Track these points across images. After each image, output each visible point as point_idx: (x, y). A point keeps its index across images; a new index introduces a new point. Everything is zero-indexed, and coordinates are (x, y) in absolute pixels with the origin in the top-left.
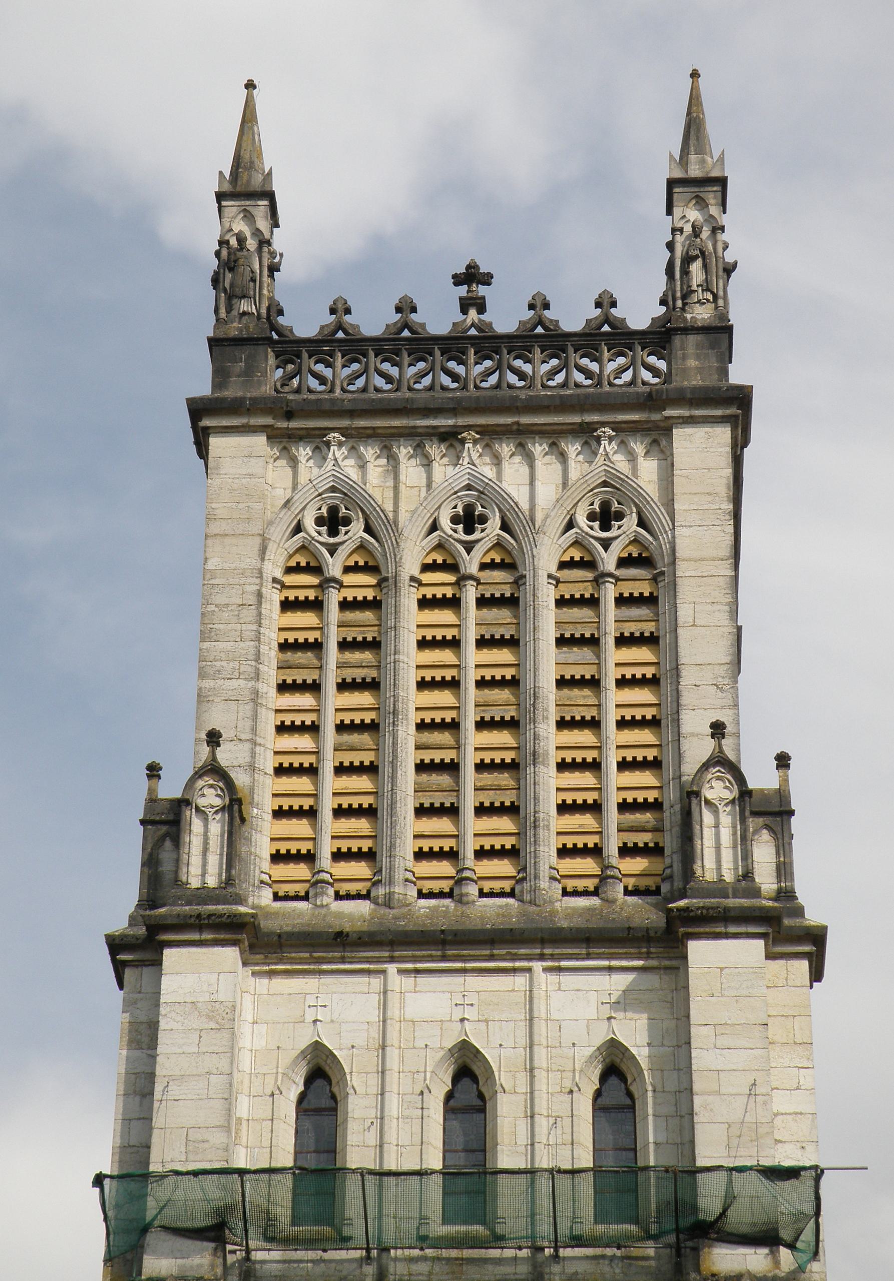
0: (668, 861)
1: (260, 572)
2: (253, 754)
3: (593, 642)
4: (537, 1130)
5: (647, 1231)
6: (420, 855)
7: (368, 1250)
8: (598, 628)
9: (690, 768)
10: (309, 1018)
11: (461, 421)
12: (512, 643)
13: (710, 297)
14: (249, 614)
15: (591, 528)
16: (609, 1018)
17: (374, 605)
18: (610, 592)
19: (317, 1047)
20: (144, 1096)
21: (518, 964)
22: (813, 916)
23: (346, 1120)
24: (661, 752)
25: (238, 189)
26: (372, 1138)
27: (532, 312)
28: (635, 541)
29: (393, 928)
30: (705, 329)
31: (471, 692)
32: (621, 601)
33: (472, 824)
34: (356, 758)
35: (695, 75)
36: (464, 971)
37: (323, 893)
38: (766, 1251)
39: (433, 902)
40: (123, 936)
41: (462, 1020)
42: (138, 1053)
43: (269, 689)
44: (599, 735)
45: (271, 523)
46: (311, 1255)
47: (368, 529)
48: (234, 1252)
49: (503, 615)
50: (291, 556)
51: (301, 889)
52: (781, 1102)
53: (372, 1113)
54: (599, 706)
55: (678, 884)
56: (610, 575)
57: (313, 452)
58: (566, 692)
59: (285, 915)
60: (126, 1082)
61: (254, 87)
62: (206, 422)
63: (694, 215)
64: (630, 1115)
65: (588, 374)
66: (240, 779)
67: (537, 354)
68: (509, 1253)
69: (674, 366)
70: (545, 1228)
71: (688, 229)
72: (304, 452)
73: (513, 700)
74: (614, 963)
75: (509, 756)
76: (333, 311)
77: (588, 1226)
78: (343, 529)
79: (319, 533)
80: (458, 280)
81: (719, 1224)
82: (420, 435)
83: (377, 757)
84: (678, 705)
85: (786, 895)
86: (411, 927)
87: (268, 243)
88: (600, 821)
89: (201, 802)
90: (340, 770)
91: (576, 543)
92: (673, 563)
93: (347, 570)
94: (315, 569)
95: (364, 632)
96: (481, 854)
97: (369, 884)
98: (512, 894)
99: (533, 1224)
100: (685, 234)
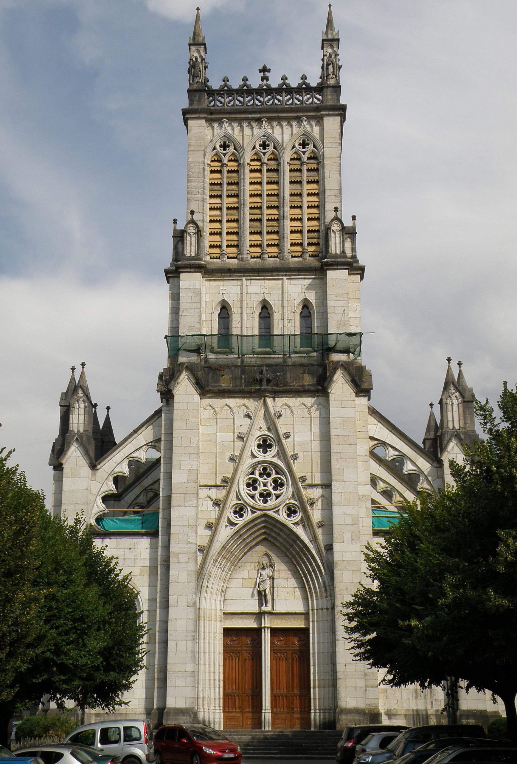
0: (321, 247)
1: (204, 162)
2: (203, 217)
3: (300, 183)
4: (285, 323)
5: (314, 349)
6: (251, 246)
7: (239, 355)
8: (302, 178)
9: (328, 220)
10: (221, 293)
11: (262, 115)
12: (277, 183)
13: (334, 77)
14: (201, 175)
15: (300, 148)
16: (305, 292)
17: (237, 172)
18: (305, 167)
19: (224, 301)
20: (176, 314)
21: (279, 277)
22: (361, 263)
23: (232, 321)
24: (319, 215)
25: (195, 43)
26: (239, 325)
27: (282, 81)
28: (313, 152)
29: (244, 267)
30: (333, 87)
31: (265, 198)
32: (308, 170)
33: (266, 237)
34: (233, 218)
35: (330, 5)
36: (264, 279)
37: (224, 257)
38: (346, 355)
39: (255, 259)
40: (169, 270)
41: (264, 293)
42: (174, 302)
43: (207, 197)
44: (302, 210)
45: (207, 147)
46: (223, 356)
47: (235, 149)
48: (202, 356)
49: (274, 174)
50: (213, 157)
51: (218, 256)
52: (351, 315)
53: (239, 319)
54: (302, 202)
55: (324, 254)
56: (305, 162)
57: (219, 125)
58: (292, 197)
59: (214, 263)
60: (171, 310)
61: (199, 9)
62: (187, 116)
63: (330, 51)
64: (310, 318)
65: (299, 100)
66: (200, 224)
67: (284, 94)
68: (277, 356)
69: (324, 98)
70: (287, 349)
71: (328, 55)
72: (216, 125)
73: (277, 200)
74: (306, 277)
75: (276, 217)
76: (224, 81)
77: (298, 348)
78: (228, 149)
79: (221, 150)
80: (260, 71)
81: (334, 348)
82: (250, 119)
83: (238, 217)
84: (325, 202)
85: (354, 257)
86: (249, 267)
87: (204, 59)
88: (302, 236)
89: (189, 231)
90: (228, 221)
91: (295, 153)
92: (323, 159)
93: (229, 161)
94: (220, 161)
95: (234, 180)
96: (268, 245)
97: (237, 254)
98: (277, 257)
99: (283, 348)
100: (327, 56)
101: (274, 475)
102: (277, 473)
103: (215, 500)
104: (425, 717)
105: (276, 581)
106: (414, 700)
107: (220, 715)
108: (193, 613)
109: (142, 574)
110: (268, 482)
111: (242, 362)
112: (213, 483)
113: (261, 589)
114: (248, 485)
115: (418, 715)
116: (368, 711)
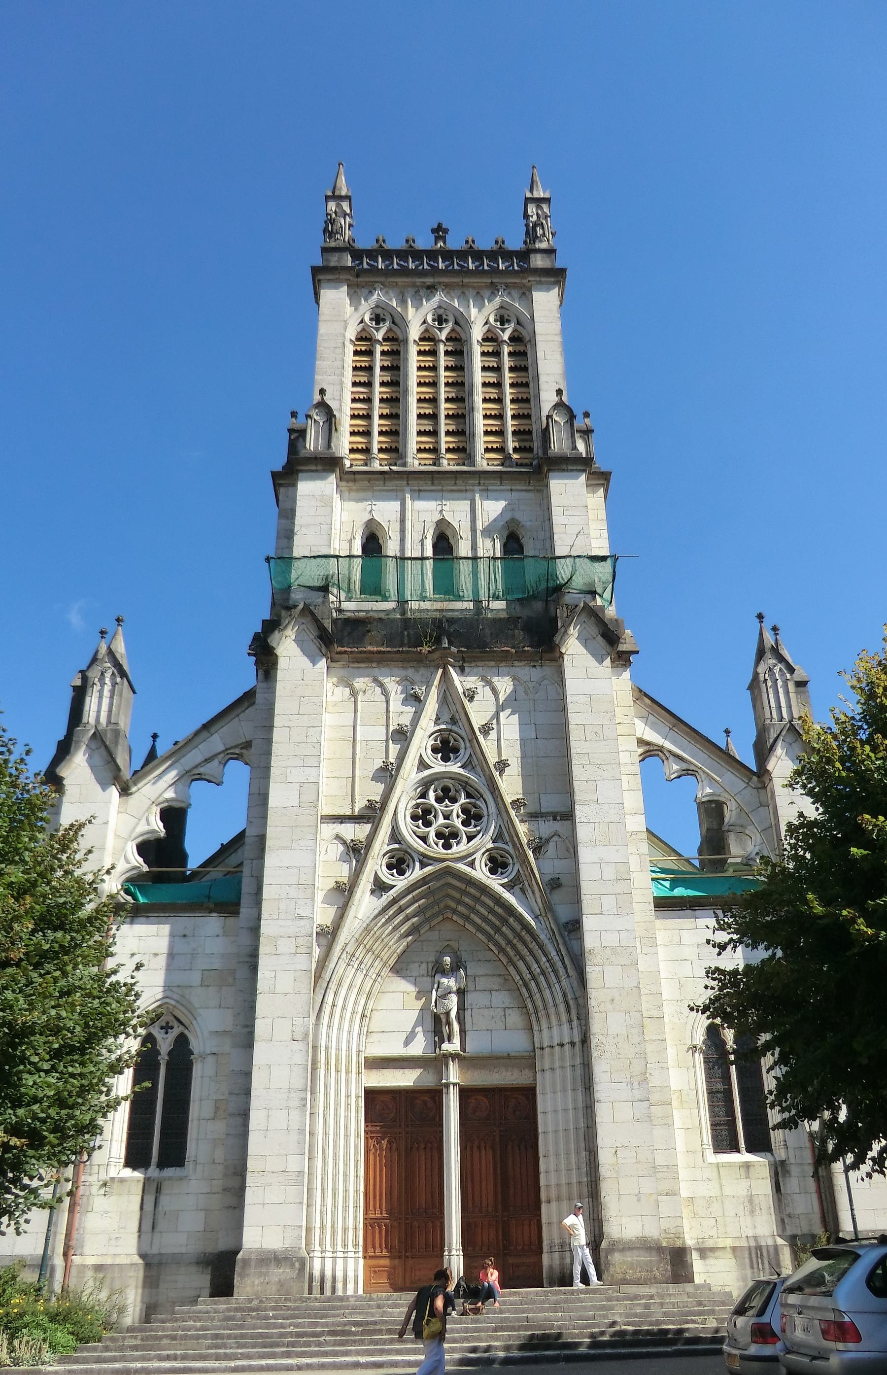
14: (339, 351)
80: (433, 231)
101: (463, 800)
102: (469, 796)
103: (352, 841)
104: (772, 1250)
105: (470, 998)
106: (749, 1219)
107: (357, 1263)
108: (304, 1053)
109: (206, 984)
110: (452, 811)
111: (403, 613)
112: (349, 813)
113: (441, 1010)
114: (414, 818)
115: (759, 1248)
116: (667, 1242)
